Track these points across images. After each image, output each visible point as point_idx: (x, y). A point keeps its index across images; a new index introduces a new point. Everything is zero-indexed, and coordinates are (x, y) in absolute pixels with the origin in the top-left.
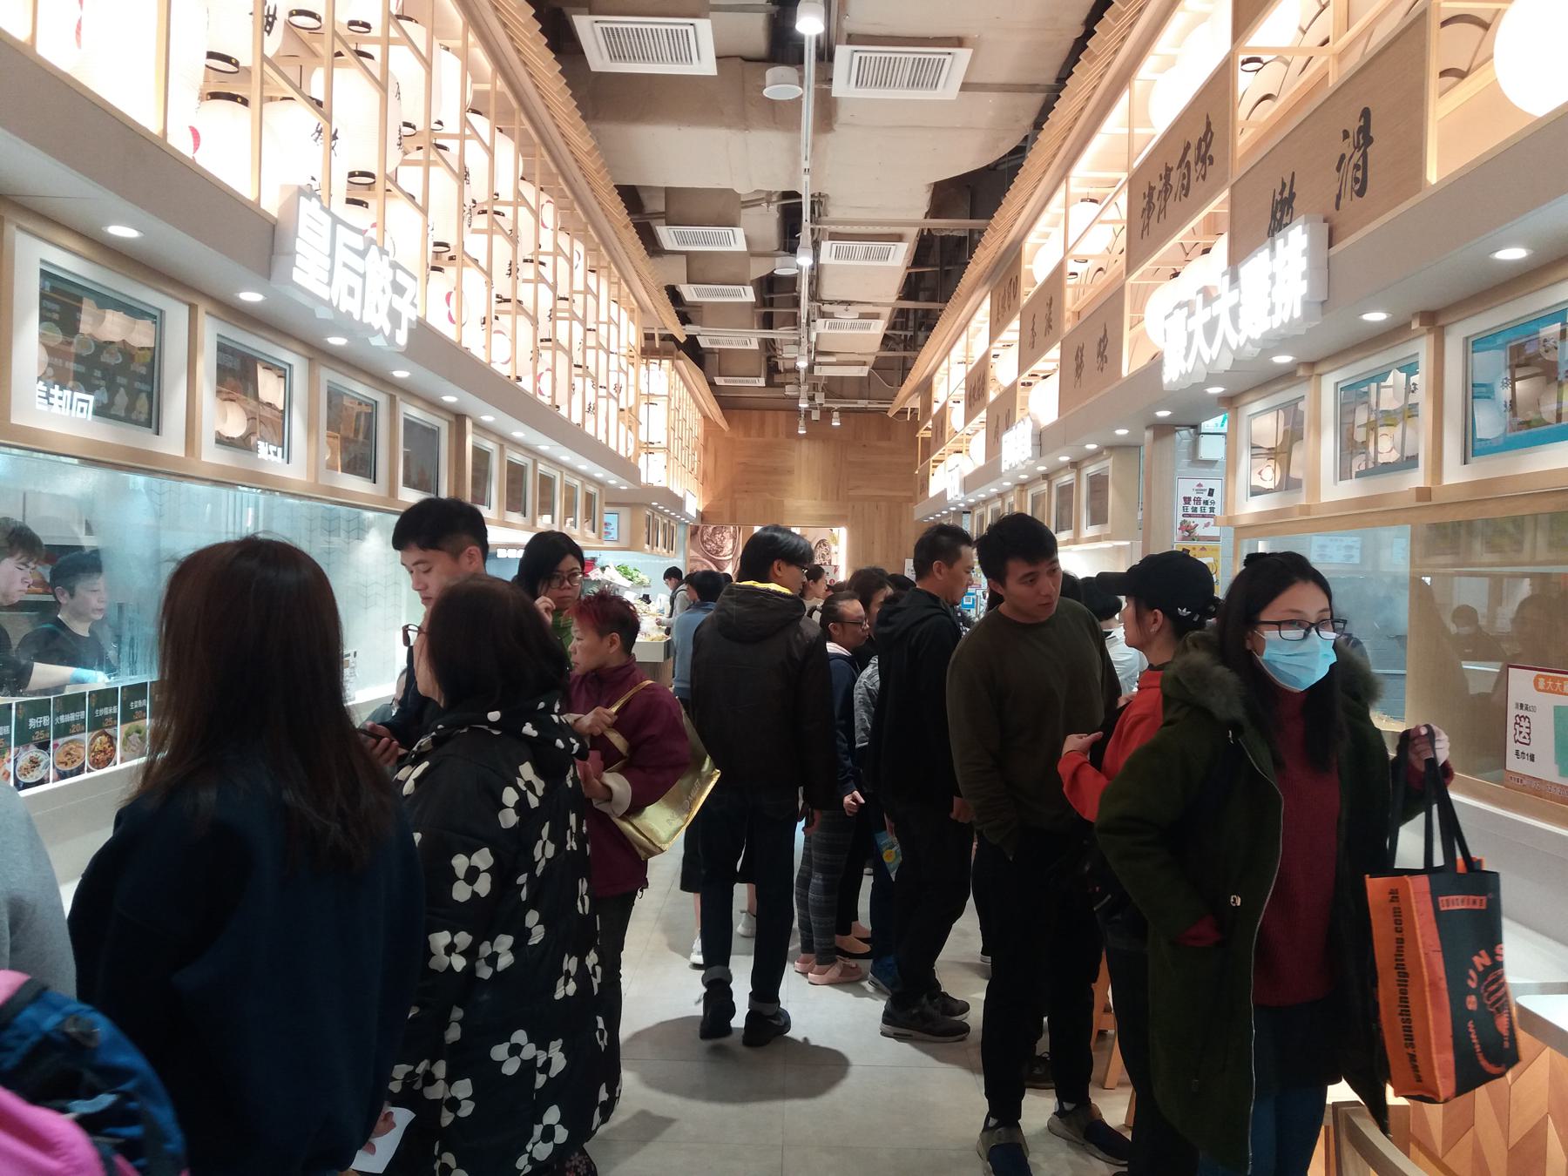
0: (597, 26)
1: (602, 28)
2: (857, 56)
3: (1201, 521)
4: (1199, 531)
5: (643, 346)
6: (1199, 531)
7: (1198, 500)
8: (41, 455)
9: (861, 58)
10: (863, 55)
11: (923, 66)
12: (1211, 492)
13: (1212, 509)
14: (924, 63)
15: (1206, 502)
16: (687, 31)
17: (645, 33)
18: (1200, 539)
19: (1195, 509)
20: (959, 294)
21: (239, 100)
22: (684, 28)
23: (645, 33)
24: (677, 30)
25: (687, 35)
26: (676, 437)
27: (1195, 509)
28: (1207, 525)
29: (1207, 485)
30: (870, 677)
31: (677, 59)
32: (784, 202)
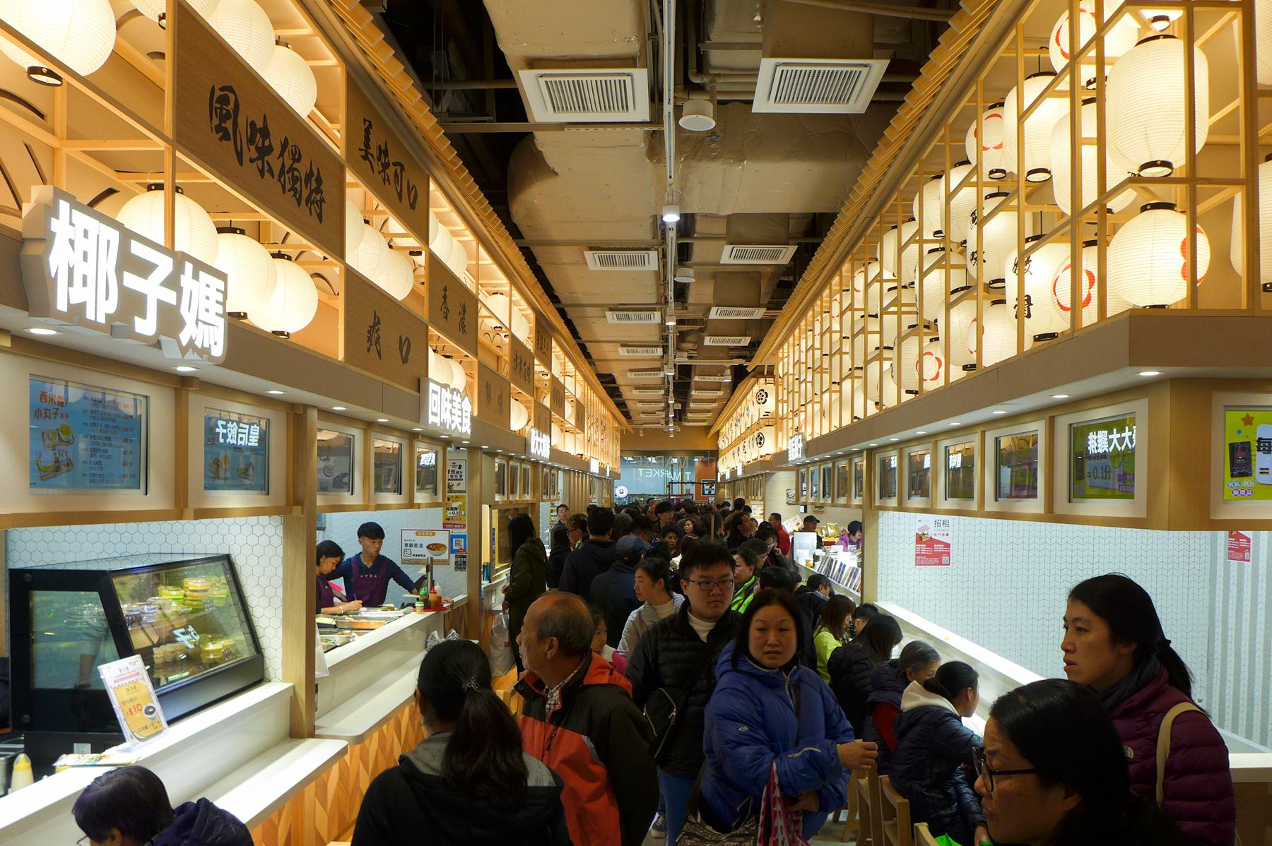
0: (542, 80)
1: (546, 82)
2: (779, 69)
3: (455, 483)
4: (455, 488)
5: (476, 414)
6: (455, 488)
7: (453, 471)
8: (827, 488)
9: (783, 71)
10: (785, 68)
11: (816, 81)
12: (460, 467)
13: (461, 476)
14: (819, 75)
15: (458, 472)
16: (624, 81)
17: (604, 85)
18: (455, 492)
19: (452, 476)
20: (805, 281)
21: (238, 232)
22: (622, 78)
23: (604, 85)
24: (606, 81)
25: (625, 86)
26: (797, 395)
27: (452, 476)
28: (459, 484)
29: (458, 463)
30: (671, 538)
31: (623, 107)
32: (681, 242)
